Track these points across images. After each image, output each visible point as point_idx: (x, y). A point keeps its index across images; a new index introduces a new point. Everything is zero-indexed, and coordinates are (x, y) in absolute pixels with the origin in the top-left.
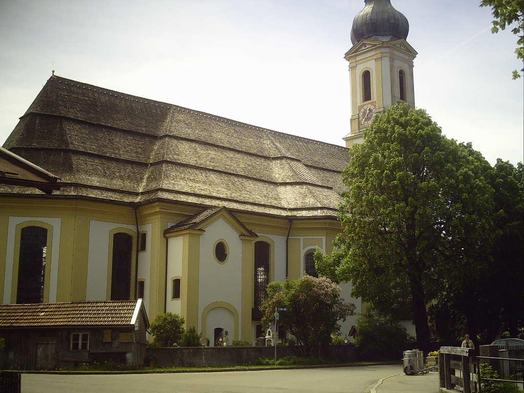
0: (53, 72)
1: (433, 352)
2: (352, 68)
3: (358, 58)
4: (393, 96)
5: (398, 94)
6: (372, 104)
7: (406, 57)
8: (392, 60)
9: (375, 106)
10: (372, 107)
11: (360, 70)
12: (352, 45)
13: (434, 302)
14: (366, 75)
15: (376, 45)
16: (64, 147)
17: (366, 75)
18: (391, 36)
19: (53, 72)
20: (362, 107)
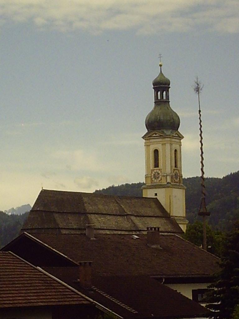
0: (42, 188)
1: (207, 305)
2: (147, 146)
3: (151, 141)
4: (171, 167)
5: (174, 165)
6: (159, 170)
7: (178, 141)
8: (171, 144)
9: (161, 172)
10: (159, 172)
11: (152, 148)
12: (147, 131)
13: (236, 277)
14: (156, 152)
15: (163, 136)
16: (57, 227)
17: (156, 152)
18: (171, 130)
19: (42, 188)
20: (153, 170)
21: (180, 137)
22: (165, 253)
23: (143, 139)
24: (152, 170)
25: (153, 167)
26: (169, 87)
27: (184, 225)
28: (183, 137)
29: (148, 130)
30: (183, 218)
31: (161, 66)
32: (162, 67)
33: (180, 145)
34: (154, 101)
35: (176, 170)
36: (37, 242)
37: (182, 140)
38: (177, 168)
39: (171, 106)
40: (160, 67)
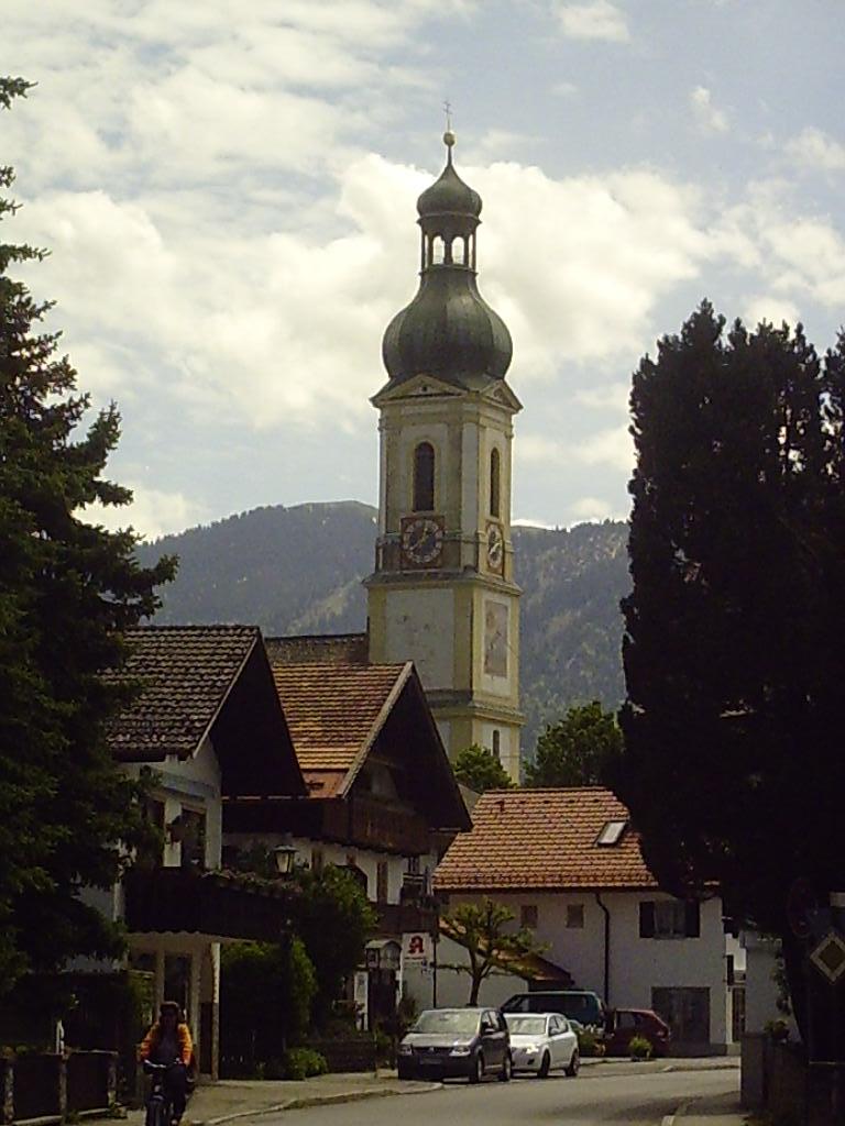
6: (434, 519)
7: (500, 417)
11: (412, 436)
14: (425, 453)
17: (425, 453)
20: (412, 520)
21: (510, 406)
22: (613, 535)
23: (376, 405)
24: (407, 522)
25: (504, 679)
26: (479, 222)
27: (443, 964)
28: (520, 407)
29: (390, 375)
30: (450, 697)
31: (449, 141)
32: (453, 148)
33: (510, 437)
34: (419, 270)
35: (495, 523)
36: (435, 734)
37: (514, 417)
38: (497, 516)
39: (482, 296)
40: (447, 147)
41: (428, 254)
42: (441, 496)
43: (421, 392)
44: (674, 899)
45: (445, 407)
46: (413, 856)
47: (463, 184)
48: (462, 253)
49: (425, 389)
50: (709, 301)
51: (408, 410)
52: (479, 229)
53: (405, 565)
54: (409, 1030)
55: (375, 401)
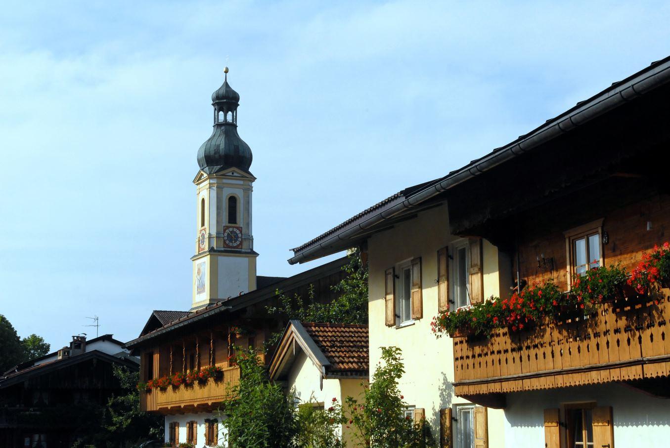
6: (238, 228)
11: (227, 192)
14: (233, 200)
17: (233, 200)
20: (228, 227)
34: (213, 124)
41: (216, 118)
42: (240, 222)
43: (231, 174)
44: (584, 432)
45: (241, 182)
46: (69, 357)
47: (223, 85)
48: (206, 182)
49: (233, 174)
50: (292, 255)
51: (225, 181)
52: (239, 108)
53: (225, 246)
54: (641, 332)
55: (239, 105)
